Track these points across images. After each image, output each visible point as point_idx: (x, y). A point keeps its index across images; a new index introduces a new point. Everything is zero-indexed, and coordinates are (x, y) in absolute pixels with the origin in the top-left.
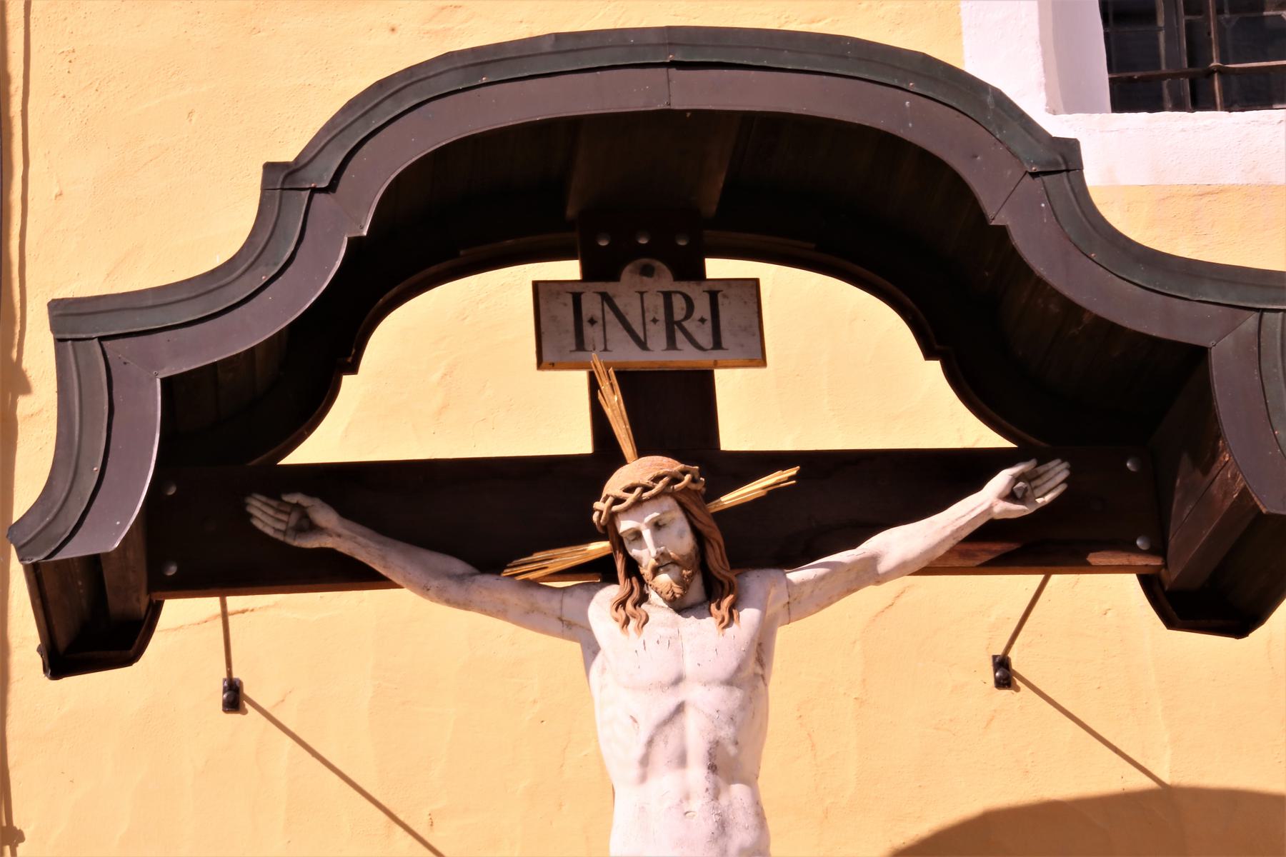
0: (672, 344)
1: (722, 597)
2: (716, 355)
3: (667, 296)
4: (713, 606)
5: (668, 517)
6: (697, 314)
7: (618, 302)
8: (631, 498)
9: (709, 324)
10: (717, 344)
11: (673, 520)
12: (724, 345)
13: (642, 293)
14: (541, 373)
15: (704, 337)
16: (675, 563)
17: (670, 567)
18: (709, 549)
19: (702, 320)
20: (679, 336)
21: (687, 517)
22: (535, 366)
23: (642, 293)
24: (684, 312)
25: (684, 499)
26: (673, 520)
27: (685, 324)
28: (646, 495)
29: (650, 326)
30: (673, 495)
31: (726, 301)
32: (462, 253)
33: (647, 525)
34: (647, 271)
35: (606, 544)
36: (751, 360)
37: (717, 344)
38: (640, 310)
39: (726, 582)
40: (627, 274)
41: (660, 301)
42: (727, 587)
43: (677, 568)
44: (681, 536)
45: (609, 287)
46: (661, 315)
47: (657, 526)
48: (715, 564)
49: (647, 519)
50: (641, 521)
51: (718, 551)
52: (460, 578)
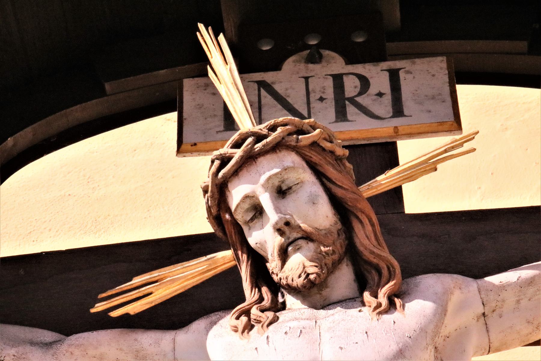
0: (341, 115)
1: (380, 285)
2: (398, 122)
3: (338, 79)
4: (367, 295)
5: (292, 178)
6: (373, 90)
7: (278, 87)
8: (238, 153)
9: (388, 99)
10: (398, 110)
11: (300, 184)
12: (406, 112)
13: (307, 79)
14: (177, 157)
15: (383, 108)
16: (308, 237)
17: (301, 242)
18: (357, 227)
19: (380, 95)
20: (351, 109)
21: (323, 184)
22: (175, 153)
23: (307, 79)
24: (358, 90)
25: (316, 158)
26: (300, 184)
27: (359, 99)
28: (259, 146)
29: (316, 105)
30: (296, 149)
31: (409, 76)
32: (107, 86)
33: (265, 186)
34: (315, 58)
35: (229, 253)
36: (441, 123)
37: (398, 110)
38: (304, 92)
39: (383, 265)
40: (289, 65)
41: (329, 83)
42: (385, 272)
43: (311, 245)
44: (313, 202)
45: (269, 77)
46: (330, 93)
47: (281, 192)
48: (366, 242)
49: (263, 178)
50: (255, 183)
51: (369, 228)
52: (48, 345)
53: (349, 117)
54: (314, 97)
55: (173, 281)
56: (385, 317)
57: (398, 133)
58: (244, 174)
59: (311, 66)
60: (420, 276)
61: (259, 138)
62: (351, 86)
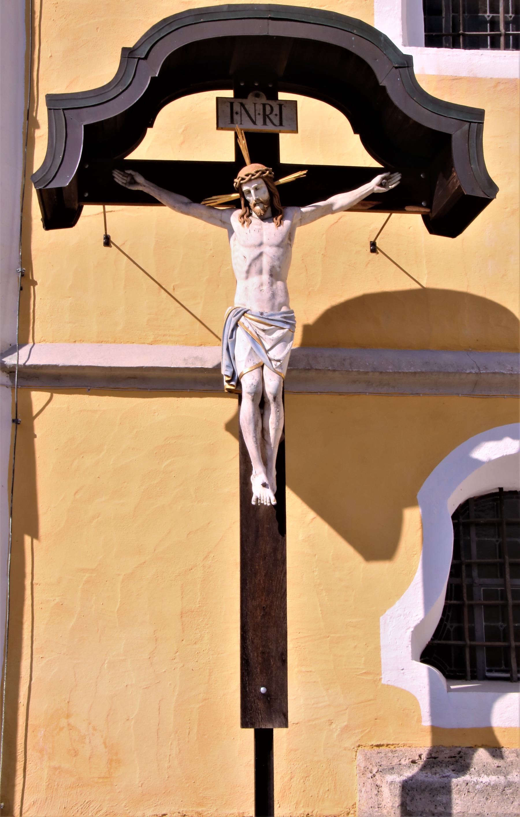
0: (265, 123)
3: (264, 105)
5: (260, 186)
6: (274, 113)
9: (278, 117)
10: (281, 124)
12: (283, 124)
18: (274, 199)
19: (276, 115)
23: (255, 104)
25: (266, 180)
26: (262, 187)
28: (253, 177)
29: (257, 116)
40: (250, 96)
41: (261, 107)
44: (264, 193)
47: (256, 189)
49: (253, 186)
50: (251, 187)
53: (267, 124)
54: (257, 112)
55: (301, 801)
56: (279, 228)
57: (281, 132)
58: (248, 184)
59: (257, 99)
60: (388, 612)
61: (253, 175)
62: (268, 108)
